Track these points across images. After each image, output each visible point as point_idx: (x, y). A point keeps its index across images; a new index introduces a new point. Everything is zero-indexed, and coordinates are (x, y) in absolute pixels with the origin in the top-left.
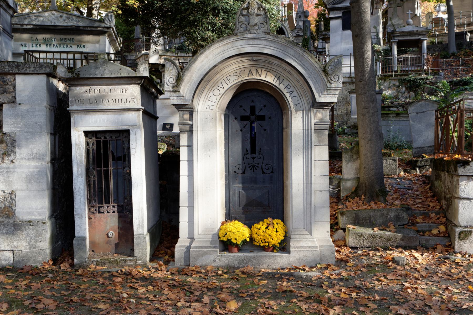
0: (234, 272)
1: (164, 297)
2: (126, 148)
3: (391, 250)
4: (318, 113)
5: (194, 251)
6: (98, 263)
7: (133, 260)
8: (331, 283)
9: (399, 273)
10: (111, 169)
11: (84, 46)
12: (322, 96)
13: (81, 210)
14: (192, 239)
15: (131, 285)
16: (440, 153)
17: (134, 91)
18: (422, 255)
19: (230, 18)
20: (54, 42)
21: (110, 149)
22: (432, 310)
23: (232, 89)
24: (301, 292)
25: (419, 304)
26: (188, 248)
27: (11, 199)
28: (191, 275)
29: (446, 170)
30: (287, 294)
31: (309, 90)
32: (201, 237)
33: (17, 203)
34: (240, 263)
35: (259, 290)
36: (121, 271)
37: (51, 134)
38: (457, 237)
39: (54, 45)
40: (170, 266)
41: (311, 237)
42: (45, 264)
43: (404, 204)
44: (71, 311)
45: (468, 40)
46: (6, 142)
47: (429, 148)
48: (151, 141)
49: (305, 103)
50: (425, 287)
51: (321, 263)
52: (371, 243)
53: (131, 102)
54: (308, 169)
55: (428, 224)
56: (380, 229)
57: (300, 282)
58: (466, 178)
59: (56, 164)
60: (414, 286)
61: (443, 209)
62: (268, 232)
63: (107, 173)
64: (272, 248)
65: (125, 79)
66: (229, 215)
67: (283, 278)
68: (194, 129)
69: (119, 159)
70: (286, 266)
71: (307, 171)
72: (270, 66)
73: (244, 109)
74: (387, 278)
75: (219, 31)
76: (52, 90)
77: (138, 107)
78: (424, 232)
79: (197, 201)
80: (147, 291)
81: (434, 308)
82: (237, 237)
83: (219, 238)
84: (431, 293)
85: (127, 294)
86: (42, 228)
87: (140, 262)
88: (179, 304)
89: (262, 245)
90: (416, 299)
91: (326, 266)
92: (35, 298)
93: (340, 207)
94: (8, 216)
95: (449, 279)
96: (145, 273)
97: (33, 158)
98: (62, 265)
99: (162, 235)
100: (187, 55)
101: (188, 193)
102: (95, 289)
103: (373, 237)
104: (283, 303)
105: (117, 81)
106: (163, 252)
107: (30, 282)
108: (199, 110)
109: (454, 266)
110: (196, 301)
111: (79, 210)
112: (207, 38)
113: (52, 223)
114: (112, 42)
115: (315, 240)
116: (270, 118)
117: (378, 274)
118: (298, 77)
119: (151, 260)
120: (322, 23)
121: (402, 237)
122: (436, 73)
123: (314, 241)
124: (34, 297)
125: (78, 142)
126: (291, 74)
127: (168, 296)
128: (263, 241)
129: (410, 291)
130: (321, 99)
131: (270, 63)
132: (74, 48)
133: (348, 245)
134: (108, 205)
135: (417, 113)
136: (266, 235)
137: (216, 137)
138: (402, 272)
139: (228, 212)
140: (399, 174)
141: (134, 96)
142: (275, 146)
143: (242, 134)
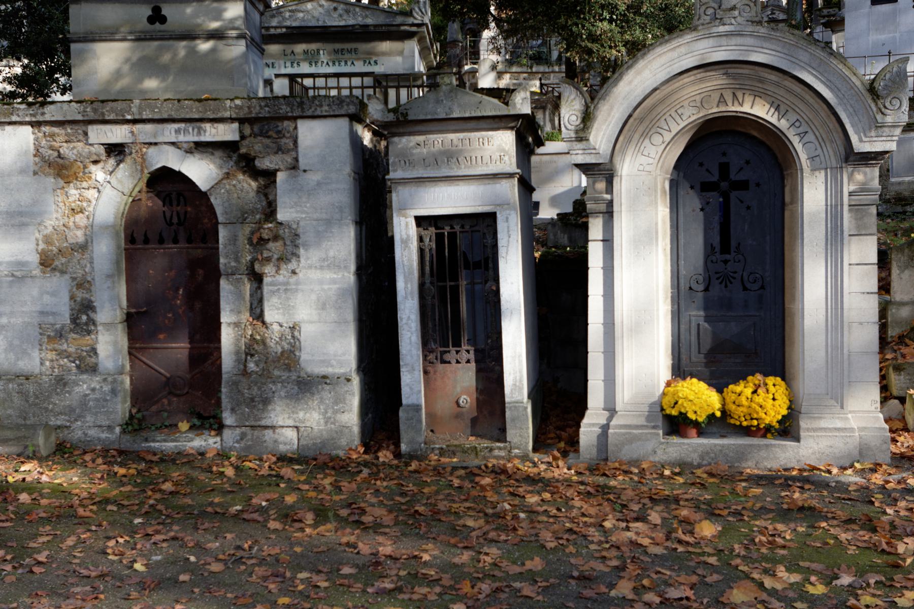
0: (693, 473)
1: (575, 512)
5: (615, 433)
6: (442, 453)
7: (505, 448)
8: (889, 496)
10: (463, 283)
11: (376, 62)
12: (864, 139)
13: (412, 356)
14: (611, 410)
15: (511, 489)
17: (503, 142)
20: (324, 57)
21: (462, 247)
24: (834, 510)
26: (605, 428)
27: (293, 337)
28: (614, 476)
30: (807, 512)
31: (839, 130)
32: (629, 408)
33: (302, 344)
34: (702, 457)
36: (486, 467)
37: (356, 223)
40: (571, 461)
41: (842, 411)
42: (351, 452)
46: (283, 239)
48: (533, 234)
49: (831, 154)
51: (861, 461)
53: (498, 163)
62: (759, 399)
63: (455, 291)
64: (762, 432)
65: (488, 121)
67: (790, 486)
68: (615, 208)
69: (477, 265)
70: (792, 465)
72: (760, 85)
73: (707, 170)
75: (622, 21)
79: (620, 341)
80: (542, 500)
82: (697, 409)
83: (662, 409)
85: (509, 504)
86: (346, 389)
87: (517, 451)
89: (745, 424)
91: (871, 466)
92: (354, 506)
93: (889, 356)
94: (288, 368)
96: (527, 468)
98: (380, 454)
100: (550, 70)
101: (605, 327)
102: (449, 495)
104: (801, 529)
105: (472, 124)
106: (552, 435)
107: (336, 480)
110: (637, 519)
111: (409, 357)
112: (601, 35)
113: (361, 381)
115: (850, 416)
116: (758, 185)
118: (816, 106)
119: (535, 450)
123: (847, 419)
124: (351, 504)
125: (405, 237)
126: (802, 99)
127: (583, 510)
130: (861, 145)
131: (761, 80)
132: (359, 67)
136: (754, 405)
137: (657, 224)
141: (503, 150)
142: (768, 238)
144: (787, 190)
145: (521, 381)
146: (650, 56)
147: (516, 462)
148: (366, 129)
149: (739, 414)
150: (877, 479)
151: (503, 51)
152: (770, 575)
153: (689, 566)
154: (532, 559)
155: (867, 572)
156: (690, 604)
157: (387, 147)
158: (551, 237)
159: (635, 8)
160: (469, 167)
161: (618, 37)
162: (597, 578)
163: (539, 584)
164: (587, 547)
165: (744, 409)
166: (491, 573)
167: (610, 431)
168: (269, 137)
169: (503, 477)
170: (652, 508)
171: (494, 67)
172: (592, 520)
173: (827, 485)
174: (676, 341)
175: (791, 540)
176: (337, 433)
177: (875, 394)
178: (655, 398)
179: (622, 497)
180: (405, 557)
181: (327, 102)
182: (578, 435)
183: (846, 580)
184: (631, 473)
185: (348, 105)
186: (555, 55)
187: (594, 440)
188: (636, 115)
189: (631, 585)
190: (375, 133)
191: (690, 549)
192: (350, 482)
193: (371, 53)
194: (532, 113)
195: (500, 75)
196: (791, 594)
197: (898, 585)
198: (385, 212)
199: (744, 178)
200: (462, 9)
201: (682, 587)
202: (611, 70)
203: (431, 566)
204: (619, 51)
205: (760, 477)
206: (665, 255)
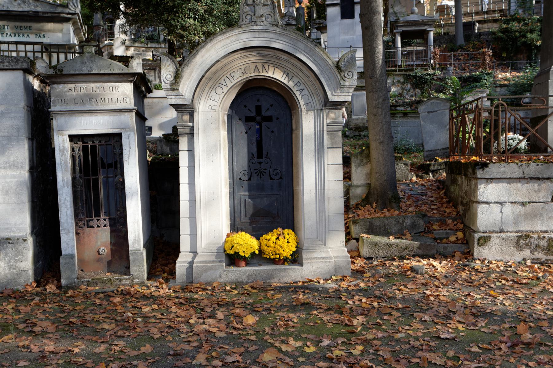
0: (243, 287)
1: (172, 315)
2: (117, 153)
3: (408, 259)
4: (330, 113)
7: (129, 279)
8: (350, 294)
9: (419, 281)
10: (101, 177)
11: (44, 36)
13: (68, 224)
14: (195, 253)
15: (133, 304)
16: (456, 155)
17: (125, 91)
18: (440, 263)
19: (215, 4)
20: (7, 30)
22: (456, 315)
23: (237, 86)
25: (442, 311)
26: (191, 263)
28: (197, 292)
29: (463, 173)
30: (307, 306)
31: (321, 88)
35: (275, 304)
36: (117, 291)
37: (29, 139)
38: (476, 243)
39: (7, 34)
40: (170, 284)
42: (27, 287)
43: (419, 211)
44: (75, 332)
45: (476, 31)
47: (442, 151)
49: (317, 102)
50: (447, 294)
52: (387, 253)
53: (122, 102)
54: (321, 173)
55: (445, 231)
56: (395, 238)
57: (316, 294)
58: (485, 180)
59: (35, 174)
60: (436, 294)
61: (460, 215)
63: (96, 182)
64: (282, 261)
65: (116, 76)
66: (234, 227)
67: (298, 291)
68: (195, 131)
69: (110, 166)
71: (320, 177)
73: (249, 109)
74: (407, 287)
76: (28, 87)
77: (131, 108)
78: (441, 239)
80: (152, 309)
81: (458, 313)
82: (244, 250)
83: (225, 251)
84: (453, 300)
85: (132, 313)
86: (23, 246)
88: (192, 321)
89: (272, 257)
90: (439, 306)
92: (28, 321)
93: (350, 216)
95: (470, 286)
96: (144, 291)
97: (10, 167)
98: (47, 287)
99: (154, 252)
102: (93, 310)
103: (389, 246)
105: (106, 78)
106: (159, 269)
107: (16, 306)
108: (200, 110)
109: (473, 273)
110: (210, 317)
112: (189, 27)
113: (34, 241)
114: (77, 31)
116: (277, 119)
117: (397, 283)
118: (309, 74)
119: (149, 279)
120: (315, 10)
121: (420, 245)
122: (443, 68)
123: (328, 252)
124: (27, 320)
126: (301, 70)
127: (177, 314)
128: (274, 253)
129: (432, 298)
130: (333, 97)
131: (278, 58)
132: (32, 38)
133: (361, 255)
134: (99, 218)
135: (429, 113)
136: (277, 246)
137: (220, 141)
138: (422, 281)
139: (233, 222)
140: (411, 180)
141: (125, 95)
143: (248, 136)
144: (294, 122)
145: (139, 237)
146: (215, 41)
147: (137, 287)
148: (35, 79)
149: (268, 251)
150: (344, 284)
151: (129, 33)
152: (285, 343)
153: (239, 342)
154: (145, 346)
155: (337, 337)
156: (239, 364)
157: (50, 91)
158: (159, 148)
159: (209, 12)
160: (104, 105)
161: (199, 29)
162: (185, 354)
163: (149, 361)
164: (179, 336)
165: (272, 249)
166: (119, 357)
167: (194, 265)
169: (128, 297)
170: (218, 310)
171: (123, 43)
172: (182, 319)
173: (317, 290)
174: (233, 210)
175: (296, 323)
176: (17, 275)
177: (342, 237)
178: (221, 244)
179: (201, 304)
180: (62, 351)
181: (7, 60)
182: (175, 269)
183: (326, 342)
184: (207, 289)
185: (22, 63)
186: (162, 37)
187: (184, 271)
188: (206, 76)
189: (205, 356)
190: (42, 82)
191: (241, 332)
192: (26, 306)
193: (41, 30)
194: (144, 72)
195: (128, 48)
196: (296, 353)
197: (353, 343)
198: (50, 132)
199: (270, 115)
200: (102, 5)
201: (235, 355)
202: (194, 47)
203: (80, 356)
204: (200, 37)
205: (281, 288)
206: (225, 160)
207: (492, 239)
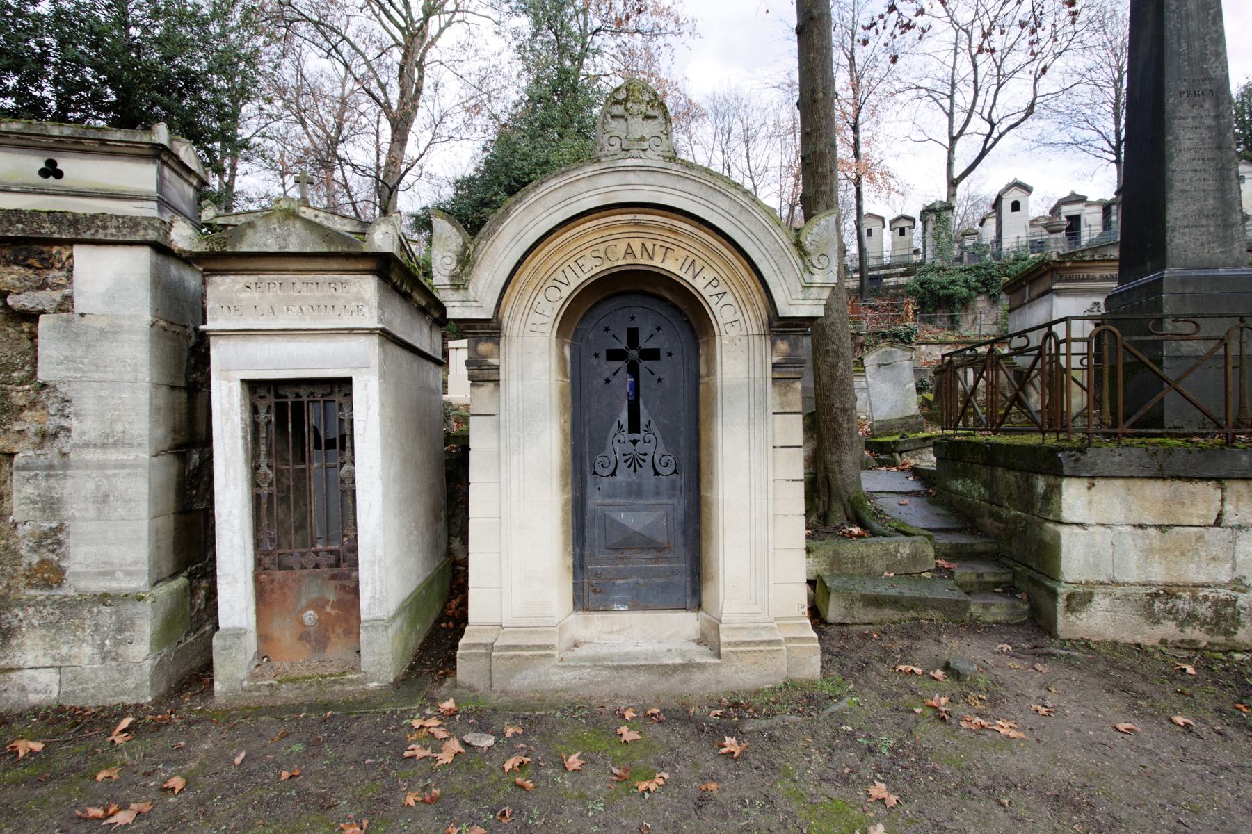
5: (501, 656)
21: (300, 418)
69: (330, 444)
77: (371, 326)
118: (737, 263)
126: (720, 256)
168: (30, 267)
185: (145, 229)
207: (1096, 599)
